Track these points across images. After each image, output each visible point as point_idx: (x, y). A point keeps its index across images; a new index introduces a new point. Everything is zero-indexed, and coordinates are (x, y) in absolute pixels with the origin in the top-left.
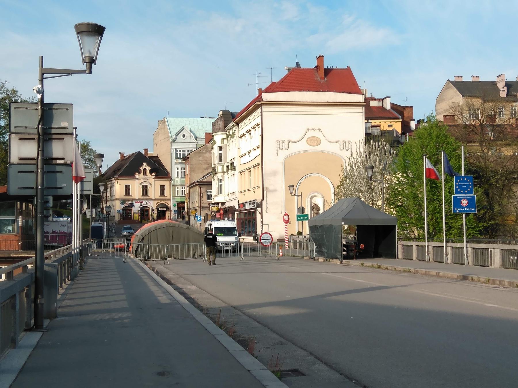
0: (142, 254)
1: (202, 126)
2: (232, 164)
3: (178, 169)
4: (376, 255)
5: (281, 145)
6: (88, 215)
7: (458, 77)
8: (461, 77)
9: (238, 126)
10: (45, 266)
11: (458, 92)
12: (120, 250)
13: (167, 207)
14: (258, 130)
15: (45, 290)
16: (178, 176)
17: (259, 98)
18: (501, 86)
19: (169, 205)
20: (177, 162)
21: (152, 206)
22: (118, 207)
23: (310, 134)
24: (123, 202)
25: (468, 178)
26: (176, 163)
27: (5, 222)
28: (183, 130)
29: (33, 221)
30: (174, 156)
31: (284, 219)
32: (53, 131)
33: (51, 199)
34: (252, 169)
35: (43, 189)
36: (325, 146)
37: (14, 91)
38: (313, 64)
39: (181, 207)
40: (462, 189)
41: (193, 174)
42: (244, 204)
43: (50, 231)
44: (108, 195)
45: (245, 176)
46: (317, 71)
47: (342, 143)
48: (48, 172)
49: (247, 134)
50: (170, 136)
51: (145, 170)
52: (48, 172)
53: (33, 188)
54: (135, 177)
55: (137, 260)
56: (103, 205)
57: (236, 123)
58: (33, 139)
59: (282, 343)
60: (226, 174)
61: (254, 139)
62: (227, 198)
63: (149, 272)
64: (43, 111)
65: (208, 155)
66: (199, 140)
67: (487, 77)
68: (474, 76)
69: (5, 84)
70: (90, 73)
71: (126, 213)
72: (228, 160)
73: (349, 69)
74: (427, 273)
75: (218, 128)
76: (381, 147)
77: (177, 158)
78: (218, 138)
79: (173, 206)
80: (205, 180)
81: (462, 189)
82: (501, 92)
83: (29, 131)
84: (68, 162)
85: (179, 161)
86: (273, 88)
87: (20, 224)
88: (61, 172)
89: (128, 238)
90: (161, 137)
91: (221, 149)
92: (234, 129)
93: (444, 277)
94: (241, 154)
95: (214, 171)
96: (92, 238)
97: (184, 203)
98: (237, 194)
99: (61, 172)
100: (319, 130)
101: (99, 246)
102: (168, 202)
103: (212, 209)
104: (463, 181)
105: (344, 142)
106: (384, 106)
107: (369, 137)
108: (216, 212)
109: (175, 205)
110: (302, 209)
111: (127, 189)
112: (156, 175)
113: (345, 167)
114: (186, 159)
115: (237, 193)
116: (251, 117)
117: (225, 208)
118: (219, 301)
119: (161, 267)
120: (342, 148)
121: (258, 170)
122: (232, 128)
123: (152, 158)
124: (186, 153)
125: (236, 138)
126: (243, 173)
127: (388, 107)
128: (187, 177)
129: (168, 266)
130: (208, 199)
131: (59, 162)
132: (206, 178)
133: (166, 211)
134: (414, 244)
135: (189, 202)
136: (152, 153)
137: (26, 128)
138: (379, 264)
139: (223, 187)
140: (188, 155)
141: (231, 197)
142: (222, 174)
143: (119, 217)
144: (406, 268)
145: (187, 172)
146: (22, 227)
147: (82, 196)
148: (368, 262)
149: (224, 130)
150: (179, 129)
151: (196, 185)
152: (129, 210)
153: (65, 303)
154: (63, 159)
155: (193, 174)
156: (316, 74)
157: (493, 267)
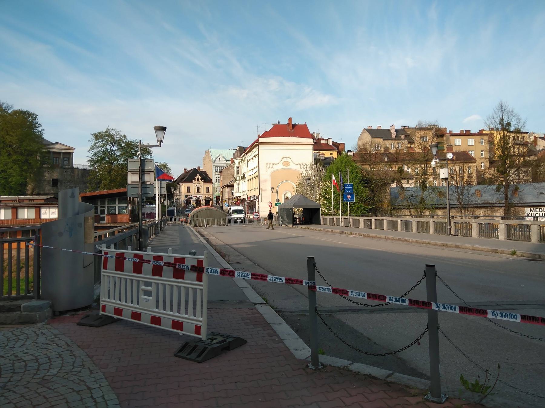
0: (193, 224)
1: (230, 154)
2: (244, 175)
3: (216, 178)
4: (311, 223)
5: (269, 166)
6: (165, 204)
7: (370, 126)
8: (371, 126)
9: (247, 155)
10: (143, 226)
11: (369, 135)
12: (183, 222)
13: (211, 199)
14: (257, 157)
15: (143, 236)
16: (216, 181)
17: (257, 141)
18: (393, 131)
19: (212, 198)
20: (216, 174)
21: (202, 198)
22: (184, 199)
23: (285, 160)
24: (186, 196)
25: (350, 185)
26: (215, 175)
27: (122, 207)
28: (219, 156)
29: (137, 207)
30: (214, 171)
31: (269, 205)
32: (145, 170)
33: (145, 198)
34: (254, 179)
35: (141, 194)
36: (292, 166)
37: (125, 136)
38: (286, 122)
39: (218, 198)
40: (347, 190)
41: (224, 180)
42: (250, 197)
43: (146, 212)
44: (178, 192)
45: (250, 182)
46: (289, 126)
47: (301, 165)
48: (144, 187)
49: (251, 159)
50: (212, 160)
51: (198, 178)
52: (144, 187)
53: (137, 194)
54: (192, 183)
55: (190, 226)
56: (175, 198)
57: (246, 153)
58: (137, 174)
59: (239, 255)
60: (241, 181)
61: (254, 163)
62: (242, 194)
63: (194, 232)
64: (141, 162)
65: (232, 170)
66: (228, 162)
67: (385, 126)
68: (378, 126)
69: (120, 133)
70: (161, 146)
71: (188, 201)
72: (242, 174)
73: (305, 125)
74: (381, 237)
75: (237, 156)
76: (318, 167)
77: (216, 172)
78: (237, 161)
79: (214, 198)
80: (231, 184)
81: (347, 190)
82: (393, 134)
83: (135, 170)
84: (152, 183)
85: (217, 173)
86: (266, 135)
87: (130, 209)
88: (149, 187)
89: (187, 216)
90: (207, 160)
91: (238, 167)
92: (245, 156)
93: (334, 232)
94: (249, 170)
95: (235, 180)
96: (168, 215)
97: (219, 196)
98: (247, 192)
99: (149, 187)
100: (289, 158)
101: (172, 220)
102: (211, 196)
103: (234, 200)
104: (348, 186)
105: (302, 164)
106: (329, 143)
107: (316, 161)
108: (236, 201)
109: (215, 198)
110: (278, 200)
111: (189, 189)
112: (204, 181)
113: (299, 178)
114: (220, 172)
115: (247, 191)
116: (253, 150)
117: (241, 199)
118: (222, 243)
119: (202, 229)
120: (301, 167)
121: (257, 179)
122: (244, 156)
123: (202, 172)
124: (221, 169)
125: (246, 162)
126: (249, 181)
127: (331, 144)
128: (221, 182)
129: (205, 229)
130: (233, 194)
131: (148, 183)
132: (231, 183)
133: (210, 201)
134: (328, 217)
135: (222, 196)
136: (202, 168)
137: (134, 169)
138: (308, 227)
139: (239, 188)
140: (222, 170)
141: (244, 193)
142: (239, 181)
143: (184, 205)
144: (320, 229)
145: (221, 180)
146: (131, 210)
147: (161, 195)
148: (304, 227)
149: (240, 157)
150: (217, 155)
151: (226, 187)
152: (190, 200)
153: (152, 243)
154: (150, 182)
155: (224, 180)
156: (288, 128)
157: (360, 228)
